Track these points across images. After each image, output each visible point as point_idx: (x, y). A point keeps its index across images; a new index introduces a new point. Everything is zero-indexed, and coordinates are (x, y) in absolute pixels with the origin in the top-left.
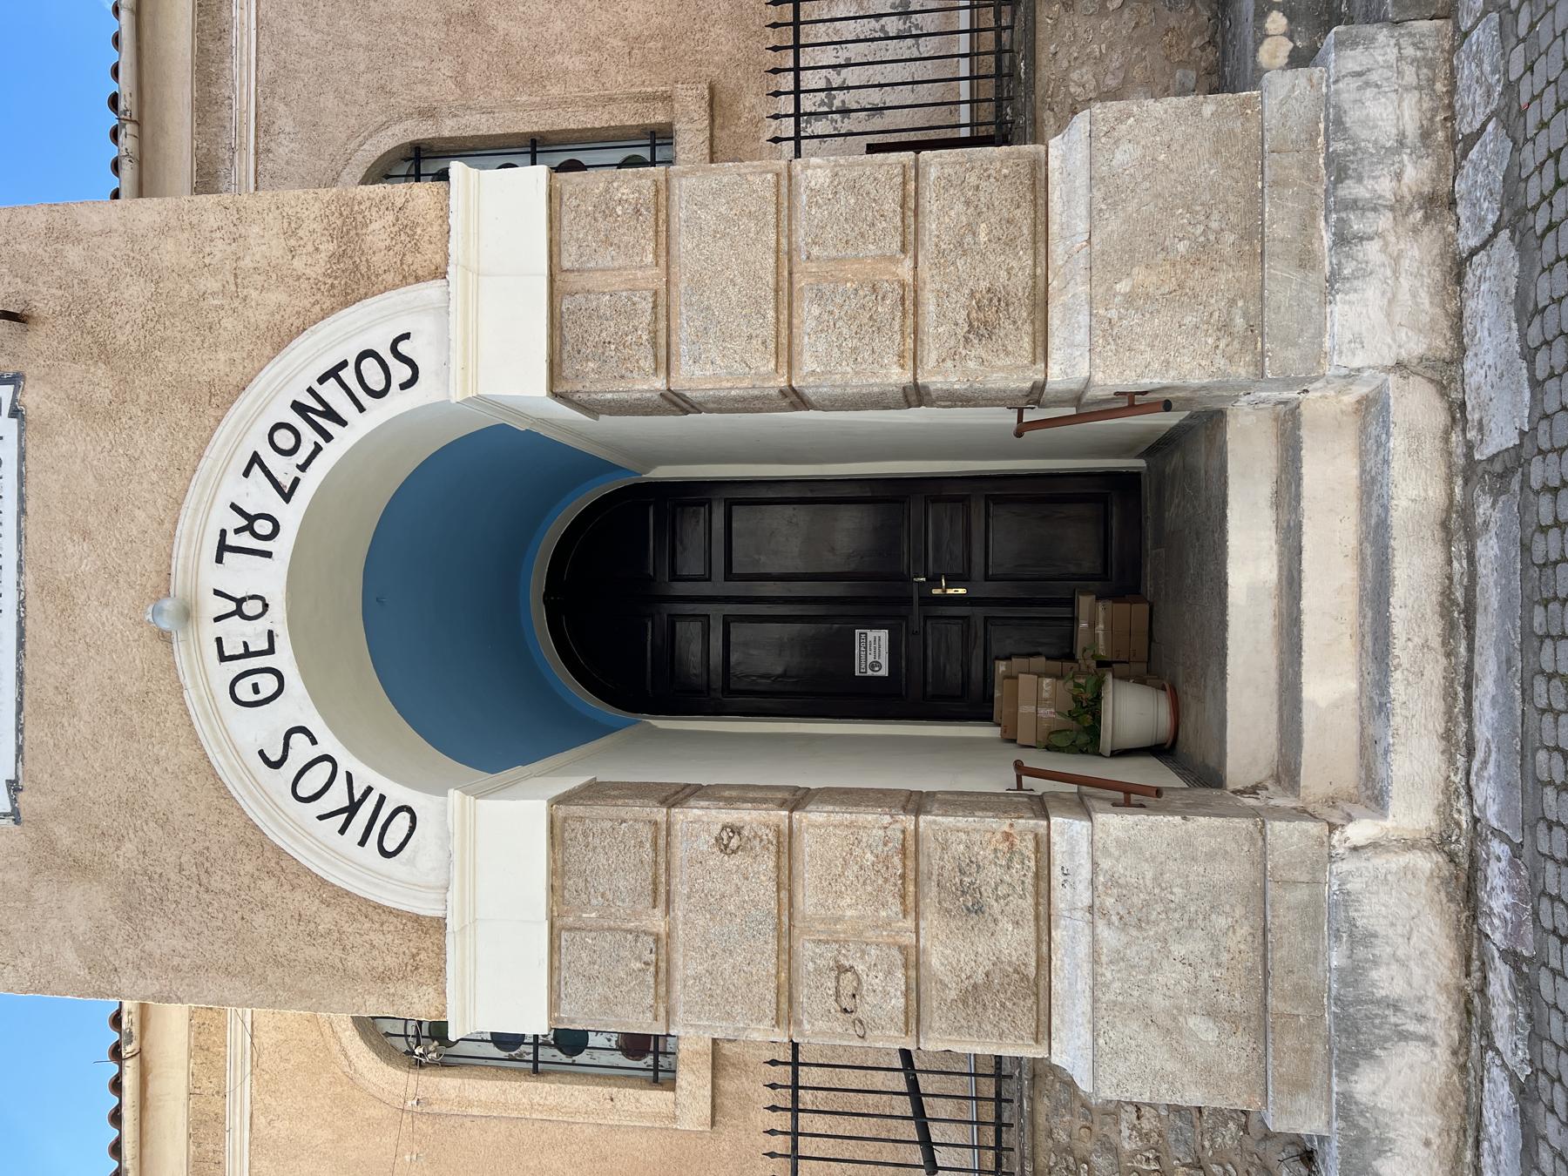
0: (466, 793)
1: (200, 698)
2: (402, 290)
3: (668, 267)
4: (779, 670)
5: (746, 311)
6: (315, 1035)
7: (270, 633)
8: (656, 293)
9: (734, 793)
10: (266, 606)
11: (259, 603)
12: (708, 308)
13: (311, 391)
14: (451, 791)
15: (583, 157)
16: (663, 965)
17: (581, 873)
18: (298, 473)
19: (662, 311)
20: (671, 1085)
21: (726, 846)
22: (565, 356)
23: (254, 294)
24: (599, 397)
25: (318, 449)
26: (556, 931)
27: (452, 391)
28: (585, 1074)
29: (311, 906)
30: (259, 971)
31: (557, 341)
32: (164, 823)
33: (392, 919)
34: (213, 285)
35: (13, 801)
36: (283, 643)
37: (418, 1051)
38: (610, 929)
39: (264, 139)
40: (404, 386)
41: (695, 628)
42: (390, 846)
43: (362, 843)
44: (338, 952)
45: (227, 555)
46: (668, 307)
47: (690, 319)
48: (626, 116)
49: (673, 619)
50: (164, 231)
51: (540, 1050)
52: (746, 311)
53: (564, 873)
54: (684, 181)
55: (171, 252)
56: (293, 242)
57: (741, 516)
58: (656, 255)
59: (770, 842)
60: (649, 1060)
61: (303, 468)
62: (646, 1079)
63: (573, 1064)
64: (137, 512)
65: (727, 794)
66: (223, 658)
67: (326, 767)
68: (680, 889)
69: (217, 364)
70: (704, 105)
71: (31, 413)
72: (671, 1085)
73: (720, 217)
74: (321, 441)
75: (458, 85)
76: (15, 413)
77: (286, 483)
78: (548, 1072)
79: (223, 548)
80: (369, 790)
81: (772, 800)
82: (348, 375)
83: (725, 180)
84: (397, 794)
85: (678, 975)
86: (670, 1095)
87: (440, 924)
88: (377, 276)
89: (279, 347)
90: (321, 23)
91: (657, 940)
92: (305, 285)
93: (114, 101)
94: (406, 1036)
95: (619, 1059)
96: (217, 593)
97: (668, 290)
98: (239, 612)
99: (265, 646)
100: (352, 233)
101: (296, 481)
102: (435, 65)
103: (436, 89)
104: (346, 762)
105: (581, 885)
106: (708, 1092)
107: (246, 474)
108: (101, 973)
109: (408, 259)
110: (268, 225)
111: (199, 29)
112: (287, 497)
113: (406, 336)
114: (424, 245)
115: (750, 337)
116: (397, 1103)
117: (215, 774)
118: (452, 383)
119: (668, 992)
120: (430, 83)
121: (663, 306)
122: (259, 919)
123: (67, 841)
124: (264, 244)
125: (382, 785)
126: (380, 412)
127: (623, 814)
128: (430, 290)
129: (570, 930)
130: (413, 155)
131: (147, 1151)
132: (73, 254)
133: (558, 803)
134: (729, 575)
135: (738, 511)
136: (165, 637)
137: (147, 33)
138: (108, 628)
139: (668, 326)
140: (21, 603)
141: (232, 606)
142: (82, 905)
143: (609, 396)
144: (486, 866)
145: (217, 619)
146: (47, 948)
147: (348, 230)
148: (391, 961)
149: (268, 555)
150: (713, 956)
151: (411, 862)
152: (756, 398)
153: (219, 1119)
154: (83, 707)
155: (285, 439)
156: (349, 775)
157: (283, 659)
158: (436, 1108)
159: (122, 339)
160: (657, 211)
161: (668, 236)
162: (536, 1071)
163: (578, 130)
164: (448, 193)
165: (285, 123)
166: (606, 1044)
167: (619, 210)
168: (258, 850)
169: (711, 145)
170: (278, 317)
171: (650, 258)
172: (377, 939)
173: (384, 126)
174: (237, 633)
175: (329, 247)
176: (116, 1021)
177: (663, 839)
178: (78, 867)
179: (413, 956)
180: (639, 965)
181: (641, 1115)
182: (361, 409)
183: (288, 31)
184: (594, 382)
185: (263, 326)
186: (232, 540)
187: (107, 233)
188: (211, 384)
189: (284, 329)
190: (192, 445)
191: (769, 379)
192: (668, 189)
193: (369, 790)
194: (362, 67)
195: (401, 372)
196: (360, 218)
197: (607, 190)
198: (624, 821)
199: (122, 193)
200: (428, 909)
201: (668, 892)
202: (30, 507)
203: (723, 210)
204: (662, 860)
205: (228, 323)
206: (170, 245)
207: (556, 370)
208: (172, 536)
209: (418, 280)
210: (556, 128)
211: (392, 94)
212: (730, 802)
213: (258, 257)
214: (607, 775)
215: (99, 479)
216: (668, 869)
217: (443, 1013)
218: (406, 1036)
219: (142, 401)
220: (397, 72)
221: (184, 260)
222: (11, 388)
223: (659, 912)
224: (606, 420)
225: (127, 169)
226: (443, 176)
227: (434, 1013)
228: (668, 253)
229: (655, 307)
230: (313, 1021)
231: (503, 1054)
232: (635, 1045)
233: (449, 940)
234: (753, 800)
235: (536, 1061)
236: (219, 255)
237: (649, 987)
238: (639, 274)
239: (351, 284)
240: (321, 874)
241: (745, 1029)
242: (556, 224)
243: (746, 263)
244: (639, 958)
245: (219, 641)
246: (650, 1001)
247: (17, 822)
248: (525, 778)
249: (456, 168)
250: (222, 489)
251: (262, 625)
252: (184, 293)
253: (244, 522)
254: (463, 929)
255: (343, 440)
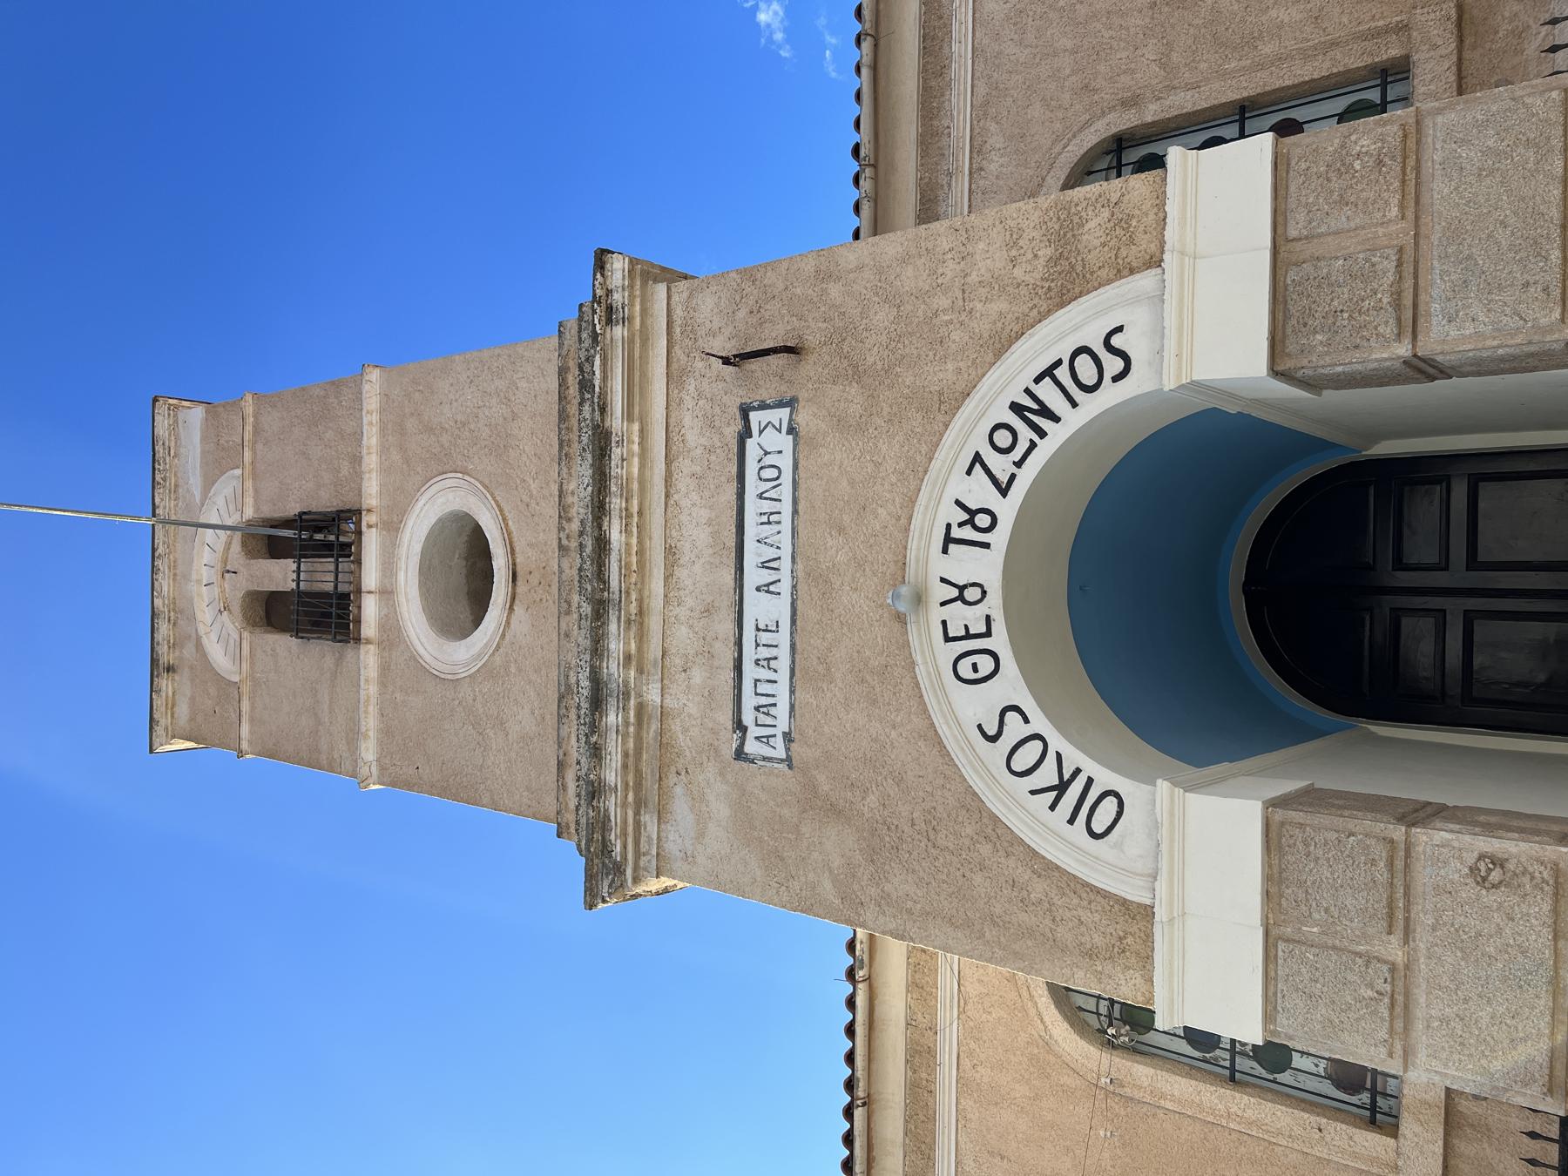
0: (1175, 784)
1: (929, 673)
2: (1117, 283)
3: (1417, 218)
4: (1542, 677)
5: (1523, 254)
6: (1014, 995)
7: (988, 618)
8: (1401, 250)
9: (1493, 819)
10: (984, 593)
11: (978, 590)
12: (1469, 257)
13: (1028, 391)
14: (1159, 781)
15: (1298, 114)
16: (1400, 999)
17: (1301, 884)
18: (1014, 469)
19: (1408, 269)
20: (1393, 1131)
21: (1484, 879)
22: (1289, 331)
23: (979, 306)
24: (1325, 371)
25: (1033, 445)
26: (1271, 940)
27: (1165, 382)
28: (1288, 1096)
29: (1023, 875)
30: (978, 927)
31: (1280, 316)
32: (899, 781)
33: (1099, 899)
34: (943, 302)
35: (788, 749)
36: (999, 627)
37: (1111, 1031)
38: (1334, 948)
39: (977, 159)
40: (1116, 379)
41: (1427, 624)
42: (1098, 828)
43: (1071, 821)
44: (1048, 922)
45: (952, 547)
46: (1416, 262)
47: (1443, 273)
48: (1354, 59)
49: (1397, 614)
50: (905, 260)
51: (1238, 1059)
52: (1523, 254)
53: (1281, 881)
54: (1440, 119)
55: (911, 278)
56: (1014, 253)
57: (1489, 496)
58: (1402, 207)
59: (1543, 881)
60: (1365, 1097)
61: (1018, 464)
62: (1361, 1118)
63: (1274, 1081)
64: (880, 510)
65: (1482, 818)
66: (948, 639)
67: (1036, 746)
68: (1423, 919)
69: (945, 374)
70: (1451, 26)
71: (802, 432)
72: (1393, 1131)
73: (1488, 151)
74: (1036, 438)
75: (1163, 66)
76: (791, 430)
77: (1004, 479)
78: (1247, 1084)
79: (949, 540)
80: (1078, 771)
81: (1548, 833)
82: (1062, 373)
83: (1494, 108)
84: (1105, 778)
85: (1419, 1013)
86: (1391, 1141)
87: (1148, 912)
88: (1092, 273)
89: (999, 354)
90: (1030, 37)
91: (1393, 968)
92: (1023, 291)
93: (856, 150)
94: (1098, 1014)
95: (1327, 1088)
96: (943, 580)
97: (1416, 244)
98: (961, 598)
99: (983, 629)
100: (1069, 235)
101: (1013, 477)
102: (1139, 52)
103: (1139, 76)
104: (1056, 742)
105: (1301, 896)
106: (1438, 1148)
107: (969, 472)
108: (848, 908)
109: (1123, 253)
110: (992, 238)
111: (924, 70)
112: (1004, 492)
113: (1119, 329)
114: (1139, 236)
115: (1527, 285)
116: (1092, 1077)
117: (940, 742)
118: (1165, 371)
119: (1406, 1029)
120: (1133, 72)
121: (1410, 264)
122: (978, 879)
123: (826, 788)
124: (989, 258)
125: (1090, 768)
126: (1092, 406)
127: (1351, 826)
128: (1145, 281)
129: (1288, 941)
130: (1115, 147)
131: (874, 1067)
132: (835, 291)
133: (1274, 805)
134: (1473, 563)
135: (1487, 492)
136: (901, 619)
137: (882, 83)
138: (857, 610)
139: (1416, 286)
140: (794, 587)
141: (955, 593)
142: (835, 845)
143: (1340, 369)
144: (1200, 864)
145: (943, 604)
146: (811, 876)
147: (1065, 233)
148: (1098, 940)
149: (986, 546)
150: (1466, 1001)
151: (1118, 846)
152: (1532, 355)
153: (931, 1052)
154: (838, 675)
155: (1003, 439)
156: (1059, 756)
157: (999, 641)
158: (1128, 1091)
159: (870, 360)
160: (1405, 158)
161: (1417, 184)
162: (1232, 1079)
163: (1294, 86)
164: (1165, 179)
165: (996, 141)
166: (1313, 1069)
167: (1357, 165)
168: (976, 816)
169: (1459, 70)
170: (999, 325)
171: (1394, 212)
172: (1086, 916)
173: (1087, 124)
174: (962, 617)
175: (1046, 252)
176: (851, 946)
177: (1401, 861)
178: (835, 812)
179: (1120, 939)
180: (1370, 993)
181: (1355, 1155)
182: (1074, 404)
183: (1000, 53)
184: (1321, 355)
185: (986, 335)
186: (956, 533)
187: (860, 268)
188: (941, 393)
189: (1005, 335)
190: (924, 449)
191: (1552, 331)
192: (1419, 131)
193: (1078, 771)
194: (1068, 71)
195: (1113, 365)
196: (1076, 219)
197: (1343, 146)
198: (1351, 834)
199: (862, 234)
200: (1137, 895)
201: (1407, 920)
202: (800, 508)
203: (1490, 143)
204: (1399, 883)
205: (955, 336)
206: (910, 271)
207: (1278, 348)
208: (907, 530)
209: (1132, 272)
210: (1268, 88)
211: (1095, 90)
212: (1490, 829)
213: (983, 271)
214: (1329, 781)
215: (852, 483)
216: (1407, 894)
217: (1151, 1000)
218: (1098, 1014)
219: (885, 413)
220: (1102, 68)
221: (921, 284)
222: (788, 410)
223: (1395, 940)
224: (1331, 396)
225: (866, 208)
226: (1157, 162)
227: (1141, 999)
228: (1417, 202)
229: (1399, 264)
230: (1012, 979)
231: (1197, 1054)
232: (1349, 1077)
233: (1157, 930)
234: (1521, 830)
235: (1232, 1069)
236: (950, 275)
237: (1383, 1019)
238: (1381, 231)
239: (1067, 283)
240: (1033, 845)
241: (1506, 1090)
242: (1282, 192)
243: (1523, 199)
244: (1371, 986)
245: (944, 623)
246: (1383, 1034)
247: (790, 767)
248: (1234, 776)
249: (1175, 155)
250: (952, 486)
251: (980, 610)
252: (920, 313)
253: (966, 517)
254: (1171, 920)
255: (1057, 434)
